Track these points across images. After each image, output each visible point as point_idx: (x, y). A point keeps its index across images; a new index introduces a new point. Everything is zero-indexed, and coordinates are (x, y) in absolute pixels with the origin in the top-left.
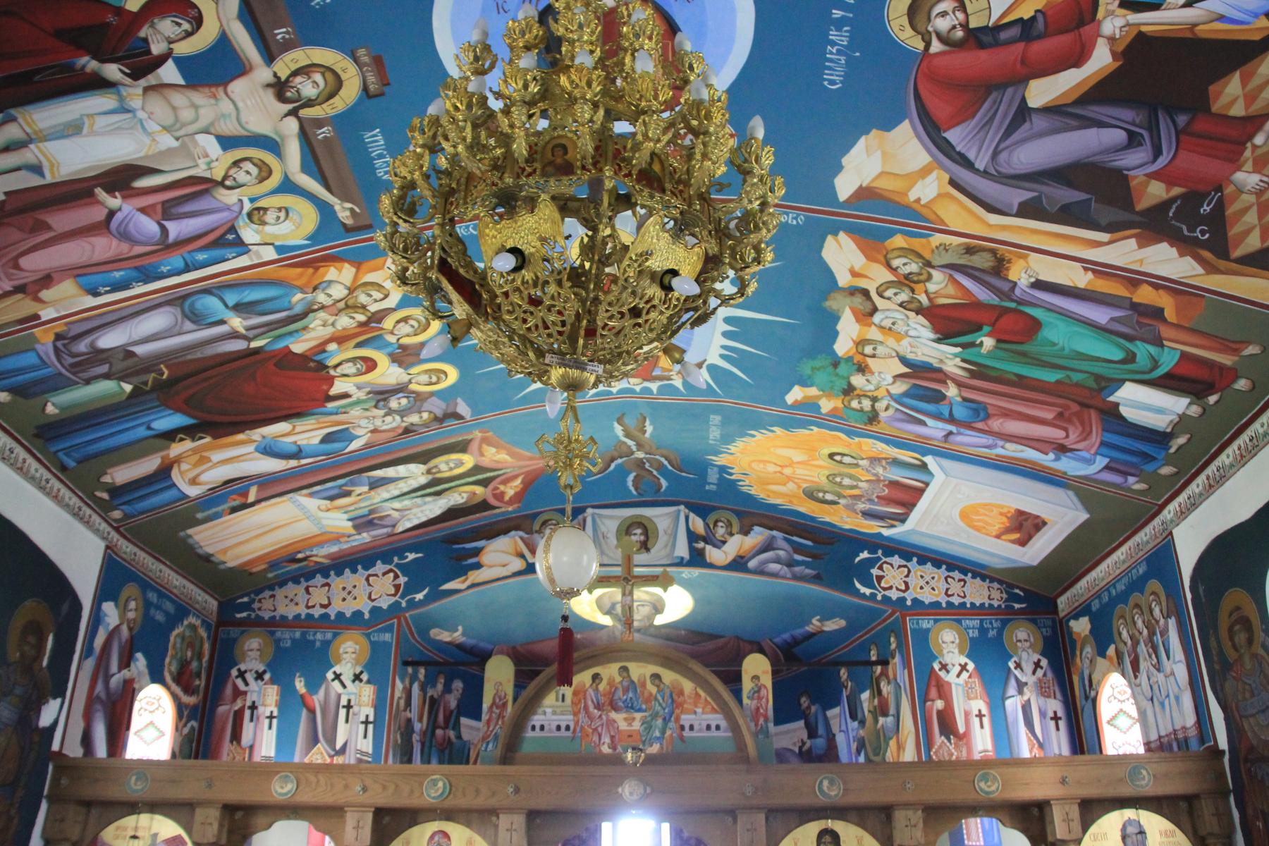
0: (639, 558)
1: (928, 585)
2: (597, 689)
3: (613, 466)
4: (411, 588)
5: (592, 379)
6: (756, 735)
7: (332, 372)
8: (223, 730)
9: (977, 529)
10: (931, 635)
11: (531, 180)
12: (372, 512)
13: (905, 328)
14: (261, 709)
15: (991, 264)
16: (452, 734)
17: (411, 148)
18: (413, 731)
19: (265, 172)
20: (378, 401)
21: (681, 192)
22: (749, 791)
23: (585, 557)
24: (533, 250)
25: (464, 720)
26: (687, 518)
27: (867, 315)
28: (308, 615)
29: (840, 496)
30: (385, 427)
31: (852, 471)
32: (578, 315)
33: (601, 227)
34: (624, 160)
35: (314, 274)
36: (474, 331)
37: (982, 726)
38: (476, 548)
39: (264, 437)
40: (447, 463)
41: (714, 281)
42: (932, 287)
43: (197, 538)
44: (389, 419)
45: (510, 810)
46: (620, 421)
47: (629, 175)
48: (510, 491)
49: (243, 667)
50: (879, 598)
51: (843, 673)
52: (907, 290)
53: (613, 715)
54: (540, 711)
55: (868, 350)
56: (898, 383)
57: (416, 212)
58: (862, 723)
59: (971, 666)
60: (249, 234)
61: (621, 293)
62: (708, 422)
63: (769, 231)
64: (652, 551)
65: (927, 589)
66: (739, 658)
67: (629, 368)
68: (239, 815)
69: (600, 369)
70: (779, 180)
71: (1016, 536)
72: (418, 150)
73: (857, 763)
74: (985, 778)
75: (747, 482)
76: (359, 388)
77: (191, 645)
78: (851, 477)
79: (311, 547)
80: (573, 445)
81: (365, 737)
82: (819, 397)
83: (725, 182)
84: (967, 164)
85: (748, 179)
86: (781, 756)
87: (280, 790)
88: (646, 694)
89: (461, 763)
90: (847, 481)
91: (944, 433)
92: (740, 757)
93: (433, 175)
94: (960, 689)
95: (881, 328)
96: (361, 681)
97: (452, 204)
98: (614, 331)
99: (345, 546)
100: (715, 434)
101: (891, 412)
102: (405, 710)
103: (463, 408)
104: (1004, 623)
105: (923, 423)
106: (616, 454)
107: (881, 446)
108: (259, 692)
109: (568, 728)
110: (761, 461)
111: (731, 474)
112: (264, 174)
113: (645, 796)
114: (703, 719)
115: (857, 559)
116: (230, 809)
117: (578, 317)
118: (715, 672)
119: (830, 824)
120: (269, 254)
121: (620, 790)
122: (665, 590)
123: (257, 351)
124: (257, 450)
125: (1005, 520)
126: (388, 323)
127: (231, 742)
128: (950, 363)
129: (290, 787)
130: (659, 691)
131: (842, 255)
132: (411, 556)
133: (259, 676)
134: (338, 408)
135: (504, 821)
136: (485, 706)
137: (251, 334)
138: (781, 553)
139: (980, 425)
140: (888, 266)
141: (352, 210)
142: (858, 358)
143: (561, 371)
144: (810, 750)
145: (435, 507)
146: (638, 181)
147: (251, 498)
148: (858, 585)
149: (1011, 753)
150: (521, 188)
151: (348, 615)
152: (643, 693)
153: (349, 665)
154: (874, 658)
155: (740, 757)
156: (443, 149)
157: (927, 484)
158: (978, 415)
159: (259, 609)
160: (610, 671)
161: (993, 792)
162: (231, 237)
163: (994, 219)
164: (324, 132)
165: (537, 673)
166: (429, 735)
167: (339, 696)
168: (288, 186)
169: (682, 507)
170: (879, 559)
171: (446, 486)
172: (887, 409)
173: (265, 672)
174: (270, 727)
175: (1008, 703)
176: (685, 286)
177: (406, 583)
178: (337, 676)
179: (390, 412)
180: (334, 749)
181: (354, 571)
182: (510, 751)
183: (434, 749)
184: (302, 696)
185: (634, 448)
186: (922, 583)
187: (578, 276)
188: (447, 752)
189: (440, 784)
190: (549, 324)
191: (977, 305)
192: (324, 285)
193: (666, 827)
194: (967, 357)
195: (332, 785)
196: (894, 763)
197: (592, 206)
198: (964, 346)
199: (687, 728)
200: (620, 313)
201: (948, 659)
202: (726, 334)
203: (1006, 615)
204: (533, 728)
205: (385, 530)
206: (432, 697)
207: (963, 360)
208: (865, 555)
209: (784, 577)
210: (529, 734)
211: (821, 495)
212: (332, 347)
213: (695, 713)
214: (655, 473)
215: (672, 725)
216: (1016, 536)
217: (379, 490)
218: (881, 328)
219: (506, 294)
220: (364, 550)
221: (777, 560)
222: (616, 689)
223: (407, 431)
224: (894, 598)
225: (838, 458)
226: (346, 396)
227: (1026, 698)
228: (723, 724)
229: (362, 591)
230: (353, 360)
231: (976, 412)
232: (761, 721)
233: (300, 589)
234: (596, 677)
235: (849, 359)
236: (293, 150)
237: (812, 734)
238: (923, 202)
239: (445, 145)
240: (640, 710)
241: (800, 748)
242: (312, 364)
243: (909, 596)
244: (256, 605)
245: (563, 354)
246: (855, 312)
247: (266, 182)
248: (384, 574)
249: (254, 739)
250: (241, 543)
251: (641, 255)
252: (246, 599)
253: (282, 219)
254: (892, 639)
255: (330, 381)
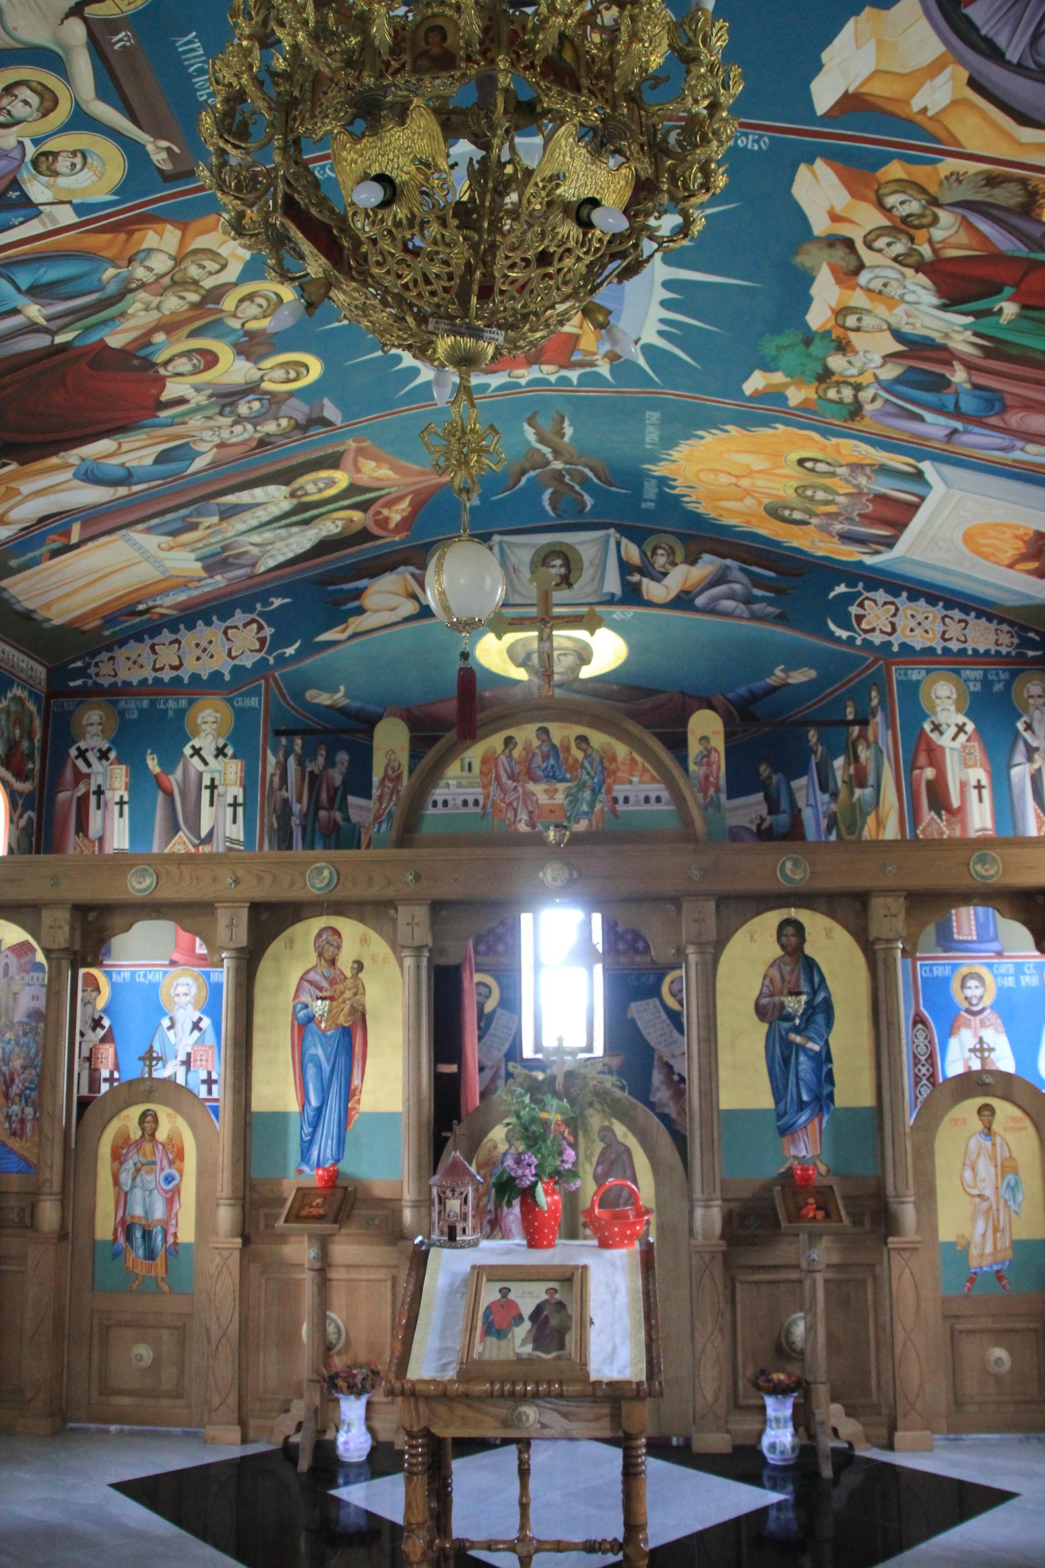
0: (560, 595)
1: (919, 627)
2: (511, 755)
3: (524, 480)
4: (280, 640)
5: (490, 351)
6: (705, 808)
7: (162, 371)
8: (66, 822)
9: (985, 556)
10: (923, 688)
11: (400, 80)
12: (225, 548)
13: (900, 291)
14: (108, 794)
15: (1019, 200)
16: (338, 816)
17: (236, 41)
18: (291, 814)
19: (49, 102)
20: (223, 407)
21: (602, 89)
22: (696, 874)
23: (488, 580)
24: (405, 177)
25: (351, 799)
26: (618, 544)
27: (850, 273)
28: (155, 679)
29: (812, 514)
30: (234, 440)
31: (829, 482)
32: (468, 264)
33: (496, 141)
34: (524, 45)
35: (128, 240)
36: (334, 293)
37: (981, 800)
38: (357, 589)
39: (83, 460)
40: (315, 483)
41: (648, 214)
42: (937, 234)
43: (13, 591)
44: (238, 429)
45: (409, 901)
46: (531, 422)
47: (532, 66)
48: (395, 516)
49: (83, 745)
50: (859, 642)
51: (812, 735)
52: (904, 239)
53: (531, 786)
54: (442, 783)
55: (851, 321)
56: (889, 366)
57: (249, 135)
58: (834, 795)
59: (970, 727)
60: (37, 190)
61: (524, 233)
62: (643, 420)
63: (721, 143)
64: (576, 586)
65: (918, 631)
66: (683, 720)
67: (538, 335)
68: (92, 916)
69: (500, 337)
70: (735, 71)
71: (1033, 565)
72: (245, 43)
73: (827, 842)
74: (982, 860)
75: (694, 498)
76: (198, 389)
77: (18, 722)
78: (826, 489)
79: (153, 596)
80: (469, 437)
81: (235, 821)
82: (787, 385)
83: (662, 75)
84: (993, 52)
85: (693, 68)
86: (735, 834)
87: (138, 886)
88: (571, 761)
89: (350, 847)
90: (820, 495)
91: (947, 432)
92: (687, 835)
93: (268, 81)
94: (956, 755)
95: (868, 291)
96: (225, 756)
97: (295, 119)
98: (517, 285)
99: (195, 593)
100: (652, 435)
101: (878, 404)
102: (280, 789)
103: (331, 412)
104: (1014, 674)
105: (920, 419)
106: (527, 465)
107: (865, 449)
108: (105, 774)
109: (476, 803)
110: (710, 470)
111: (674, 488)
112: (48, 104)
113: (571, 882)
114: (639, 788)
115: (832, 595)
116: (81, 910)
117: (469, 268)
118: (655, 734)
119: (793, 913)
120: (67, 216)
121: (541, 875)
122: (592, 633)
123: (65, 347)
124: (76, 476)
125: (1021, 544)
126: (229, 303)
127: (77, 834)
128: (959, 337)
129: (148, 882)
130: (586, 756)
131: (819, 192)
132: (277, 602)
133: (103, 755)
134: (174, 417)
135: (403, 914)
136: (376, 780)
137: (54, 325)
138: (737, 587)
139: (993, 421)
140: (880, 205)
141: (169, 150)
142: (837, 332)
143: (450, 340)
144: (771, 826)
145: (303, 540)
146: (544, 75)
147: (74, 539)
148: (832, 626)
149: (1015, 827)
150: (385, 89)
151: (205, 677)
152: (567, 760)
153: (210, 737)
154: (850, 717)
155: (687, 835)
156: (279, 41)
157: (922, 499)
158: (994, 404)
159: (97, 675)
160: (526, 734)
161: (992, 876)
162: (13, 195)
163: (1028, 134)
164: (121, 39)
165: (436, 739)
166: (311, 815)
167: (200, 775)
168: (81, 120)
169: (612, 531)
170: (860, 594)
171: (316, 512)
172: (873, 400)
173: (109, 750)
174: (121, 815)
175: (1014, 772)
176: (610, 220)
177: (272, 635)
178: (197, 752)
179: (239, 420)
180: (198, 837)
181: (208, 623)
182: (407, 832)
183: (317, 834)
184: (156, 777)
185: (550, 457)
186: (912, 623)
187: (468, 213)
188: (333, 837)
189: (326, 873)
190: (432, 278)
191: (996, 258)
192: (142, 255)
193: (597, 918)
194: (982, 330)
195: (198, 878)
196: (872, 842)
197: (482, 114)
198: (978, 315)
199: (621, 801)
200: (524, 260)
201: (941, 718)
202: (665, 304)
203: (1017, 665)
204: (435, 804)
205: (241, 572)
206: (311, 773)
207: (976, 334)
208: (841, 589)
209: (740, 617)
210: (430, 811)
211: (787, 513)
212: (159, 338)
213: (631, 782)
214: (577, 488)
215: (602, 797)
216: (1033, 565)
217: (234, 520)
218: (868, 291)
219: (374, 242)
220: (215, 599)
221: (732, 596)
222: (534, 754)
223: (263, 443)
224: (877, 642)
225: (809, 465)
226: (181, 401)
227: (1036, 766)
228: (665, 795)
229: (220, 649)
230: (188, 354)
231: (990, 403)
232: (712, 791)
233: (144, 648)
234: (509, 741)
235: (826, 334)
236: (82, 66)
237: (773, 808)
238: (930, 113)
239: (280, 33)
240: (563, 780)
241: (759, 826)
242: (136, 362)
243: (896, 641)
244: (92, 671)
245: (452, 318)
246: (835, 270)
247: (52, 115)
248: (245, 626)
249: (104, 828)
250: (67, 595)
251: (551, 179)
252: (79, 664)
253: (79, 167)
254: (874, 694)
255: (160, 383)
